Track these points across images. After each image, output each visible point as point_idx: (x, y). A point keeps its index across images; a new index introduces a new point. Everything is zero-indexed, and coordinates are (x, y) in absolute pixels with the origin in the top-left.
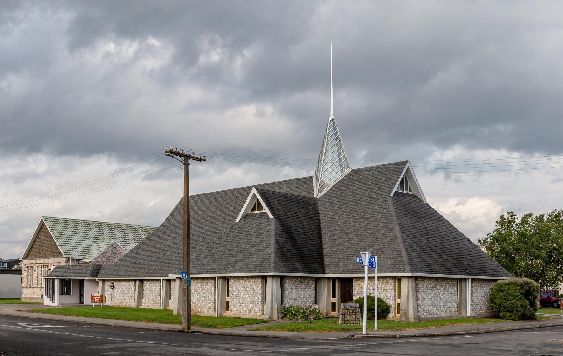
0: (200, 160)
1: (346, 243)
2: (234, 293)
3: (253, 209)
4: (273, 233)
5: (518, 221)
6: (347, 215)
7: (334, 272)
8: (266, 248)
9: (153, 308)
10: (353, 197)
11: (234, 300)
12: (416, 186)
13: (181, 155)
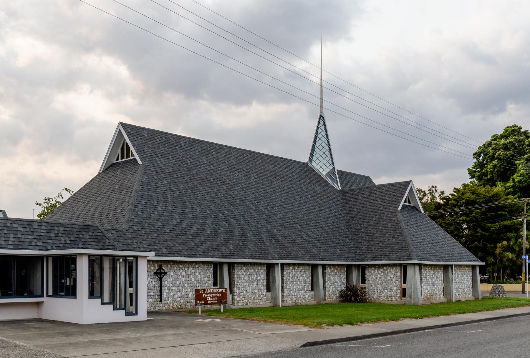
9: (253, 306)
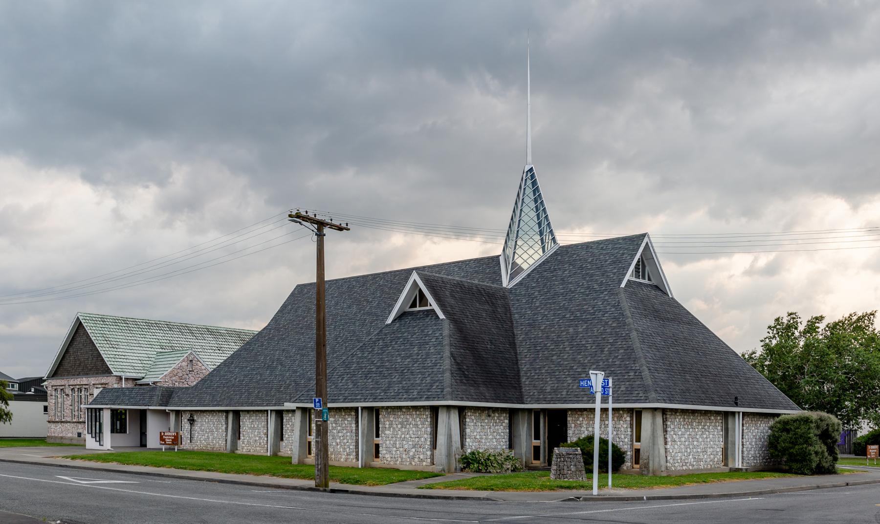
0: (340, 229)
1: (555, 357)
2: (387, 432)
3: (414, 305)
4: (446, 341)
5: (801, 328)
6: (554, 315)
7: (538, 401)
8: (435, 365)
9: (255, 454)
10: (563, 288)
11: (388, 442)
12: (657, 272)
13: (313, 221)
